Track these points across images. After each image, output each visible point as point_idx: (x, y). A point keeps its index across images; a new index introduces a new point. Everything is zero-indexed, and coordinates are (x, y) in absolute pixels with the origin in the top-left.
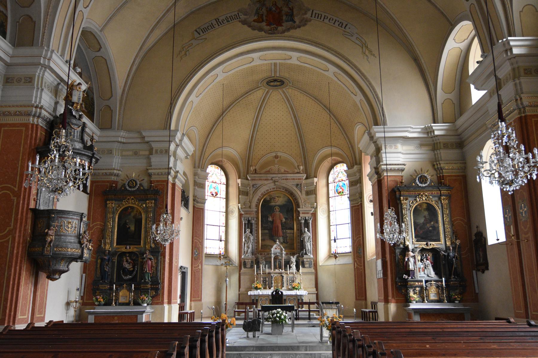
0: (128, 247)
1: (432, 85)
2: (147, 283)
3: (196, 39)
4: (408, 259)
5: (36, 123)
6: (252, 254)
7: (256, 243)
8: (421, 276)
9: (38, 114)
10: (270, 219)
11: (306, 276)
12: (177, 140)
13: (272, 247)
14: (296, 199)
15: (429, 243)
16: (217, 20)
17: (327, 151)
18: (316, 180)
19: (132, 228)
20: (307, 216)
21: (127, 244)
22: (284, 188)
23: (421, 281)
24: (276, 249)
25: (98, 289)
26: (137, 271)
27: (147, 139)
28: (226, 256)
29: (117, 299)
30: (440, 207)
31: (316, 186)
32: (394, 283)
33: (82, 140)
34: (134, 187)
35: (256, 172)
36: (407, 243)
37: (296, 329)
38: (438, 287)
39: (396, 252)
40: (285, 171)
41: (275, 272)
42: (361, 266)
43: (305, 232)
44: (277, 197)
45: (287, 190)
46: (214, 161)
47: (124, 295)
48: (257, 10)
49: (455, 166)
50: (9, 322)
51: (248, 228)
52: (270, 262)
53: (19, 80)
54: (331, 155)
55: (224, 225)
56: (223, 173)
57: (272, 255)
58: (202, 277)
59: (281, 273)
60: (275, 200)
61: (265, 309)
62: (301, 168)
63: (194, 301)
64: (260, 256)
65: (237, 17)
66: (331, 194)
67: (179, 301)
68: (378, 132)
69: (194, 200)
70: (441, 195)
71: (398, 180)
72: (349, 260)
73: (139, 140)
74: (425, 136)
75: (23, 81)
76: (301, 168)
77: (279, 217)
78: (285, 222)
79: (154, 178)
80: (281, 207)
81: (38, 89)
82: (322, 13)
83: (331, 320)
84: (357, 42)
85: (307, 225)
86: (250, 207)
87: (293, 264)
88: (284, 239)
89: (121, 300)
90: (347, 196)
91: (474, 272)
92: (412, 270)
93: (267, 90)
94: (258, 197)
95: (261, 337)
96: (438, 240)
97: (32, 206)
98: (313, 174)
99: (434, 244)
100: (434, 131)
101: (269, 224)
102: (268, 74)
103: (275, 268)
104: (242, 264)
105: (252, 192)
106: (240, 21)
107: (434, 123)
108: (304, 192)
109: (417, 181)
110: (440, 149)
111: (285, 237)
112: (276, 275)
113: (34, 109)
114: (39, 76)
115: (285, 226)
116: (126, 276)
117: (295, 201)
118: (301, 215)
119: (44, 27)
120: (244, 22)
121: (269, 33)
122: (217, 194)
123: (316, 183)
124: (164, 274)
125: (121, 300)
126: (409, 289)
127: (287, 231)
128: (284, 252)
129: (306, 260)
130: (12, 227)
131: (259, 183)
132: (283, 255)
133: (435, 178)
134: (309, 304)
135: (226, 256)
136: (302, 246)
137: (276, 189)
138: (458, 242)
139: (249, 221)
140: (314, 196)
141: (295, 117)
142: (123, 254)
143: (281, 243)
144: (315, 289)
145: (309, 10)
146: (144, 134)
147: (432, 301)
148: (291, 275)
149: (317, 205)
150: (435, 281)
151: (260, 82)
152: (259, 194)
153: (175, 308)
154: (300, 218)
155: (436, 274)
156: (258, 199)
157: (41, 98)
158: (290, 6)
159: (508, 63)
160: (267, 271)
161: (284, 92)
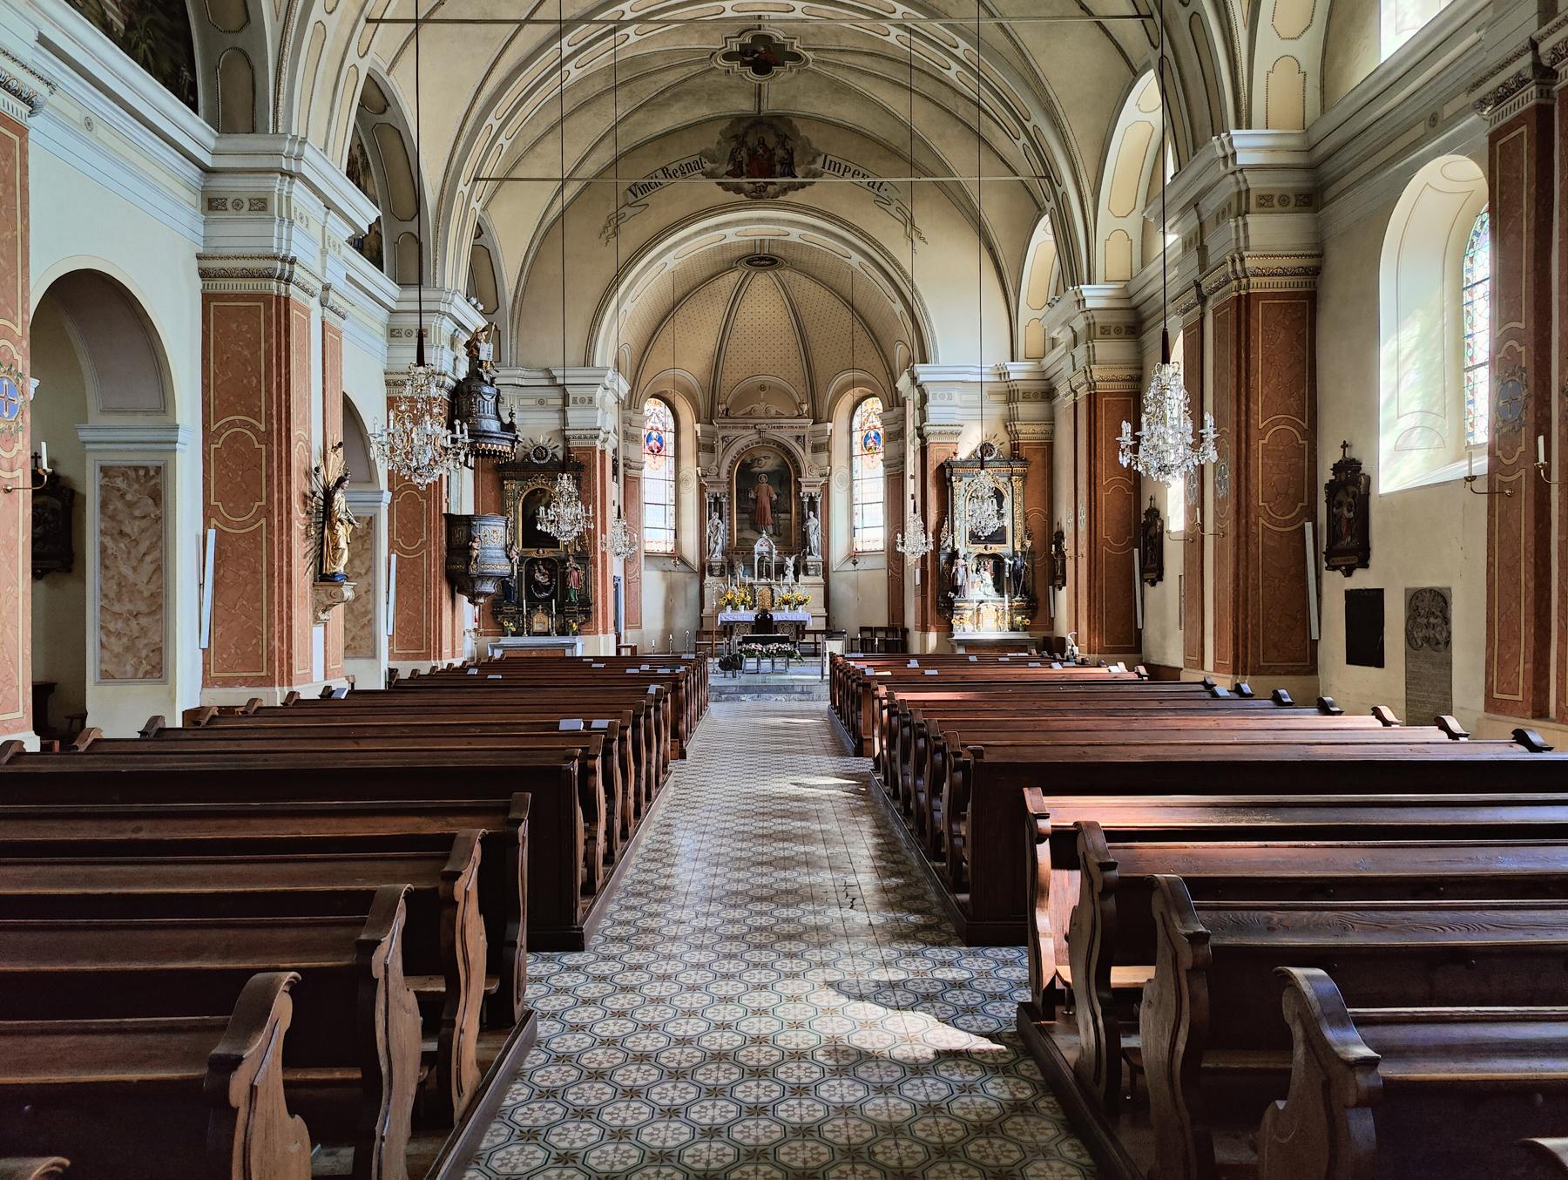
0: (541, 551)
1: (1012, 294)
3: (630, 206)
5: (276, 292)
7: (729, 535)
9: (286, 274)
10: (752, 495)
13: (755, 542)
14: (795, 462)
15: (989, 546)
16: (665, 170)
17: (847, 377)
18: (830, 426)
20: (815, 491)
21: (539, 547)
26: (556, 586)
28: (677, 556)
29: (530, 625)
30: (1010, 492)
33: (499, 418)
34: (543, 459)
35: (727, 415)
36: (957, 546)
42: (898, 573)
43: (809, 517)
45: (780, 445)
46: (657, 391)
47: (540, 621)
48: (732, 153)
49: (1038, 429)
51: (715, 511)
53: (238, 205)
54: (853, 384)
56: (668, 412)
59: (770, 585)
62: (805, 407)
66: (857, 450)
67: (613, 628)
70: (1012, 475)
72: (882, 562)
73: (546, 382)
74: (997, 379)
75: (247, 205)
76: (805, 407)
77: (767, 493)
78: (777, 500)
81: (282, 220)
82: (840, 161)
84: (898, 216)
86: (718, 475)
88: (774, 529)
89: (537, 628)
90: (881, 456)
94: (731, 458)
95: (744, 677)
97: (445, 511)
98: (825, 416)
101: (750, 503)
103: (760, 576)
105: (720, 450)
108: (809, 450)
110: (1247, 212)
112: (761, 588)
114: (280, 196)
116: (541, 593)
120: (710, 175)
121: (752, 197)
124: (596, 591)
125: (537, 628)
128: (775, 552)
130: (425, 539)
131: (735, 433)
132: (774, 556)
133: (1007, 445)
134: (815, 632)
140: (827, 454)
142: (534, 561)
145: (820, 155)
150: (992, 601)
152: (733, 451)
154: (801, 494)
156: (732, 462)
157: (289, 240)
158: (789, 148)
161: (776, 275)
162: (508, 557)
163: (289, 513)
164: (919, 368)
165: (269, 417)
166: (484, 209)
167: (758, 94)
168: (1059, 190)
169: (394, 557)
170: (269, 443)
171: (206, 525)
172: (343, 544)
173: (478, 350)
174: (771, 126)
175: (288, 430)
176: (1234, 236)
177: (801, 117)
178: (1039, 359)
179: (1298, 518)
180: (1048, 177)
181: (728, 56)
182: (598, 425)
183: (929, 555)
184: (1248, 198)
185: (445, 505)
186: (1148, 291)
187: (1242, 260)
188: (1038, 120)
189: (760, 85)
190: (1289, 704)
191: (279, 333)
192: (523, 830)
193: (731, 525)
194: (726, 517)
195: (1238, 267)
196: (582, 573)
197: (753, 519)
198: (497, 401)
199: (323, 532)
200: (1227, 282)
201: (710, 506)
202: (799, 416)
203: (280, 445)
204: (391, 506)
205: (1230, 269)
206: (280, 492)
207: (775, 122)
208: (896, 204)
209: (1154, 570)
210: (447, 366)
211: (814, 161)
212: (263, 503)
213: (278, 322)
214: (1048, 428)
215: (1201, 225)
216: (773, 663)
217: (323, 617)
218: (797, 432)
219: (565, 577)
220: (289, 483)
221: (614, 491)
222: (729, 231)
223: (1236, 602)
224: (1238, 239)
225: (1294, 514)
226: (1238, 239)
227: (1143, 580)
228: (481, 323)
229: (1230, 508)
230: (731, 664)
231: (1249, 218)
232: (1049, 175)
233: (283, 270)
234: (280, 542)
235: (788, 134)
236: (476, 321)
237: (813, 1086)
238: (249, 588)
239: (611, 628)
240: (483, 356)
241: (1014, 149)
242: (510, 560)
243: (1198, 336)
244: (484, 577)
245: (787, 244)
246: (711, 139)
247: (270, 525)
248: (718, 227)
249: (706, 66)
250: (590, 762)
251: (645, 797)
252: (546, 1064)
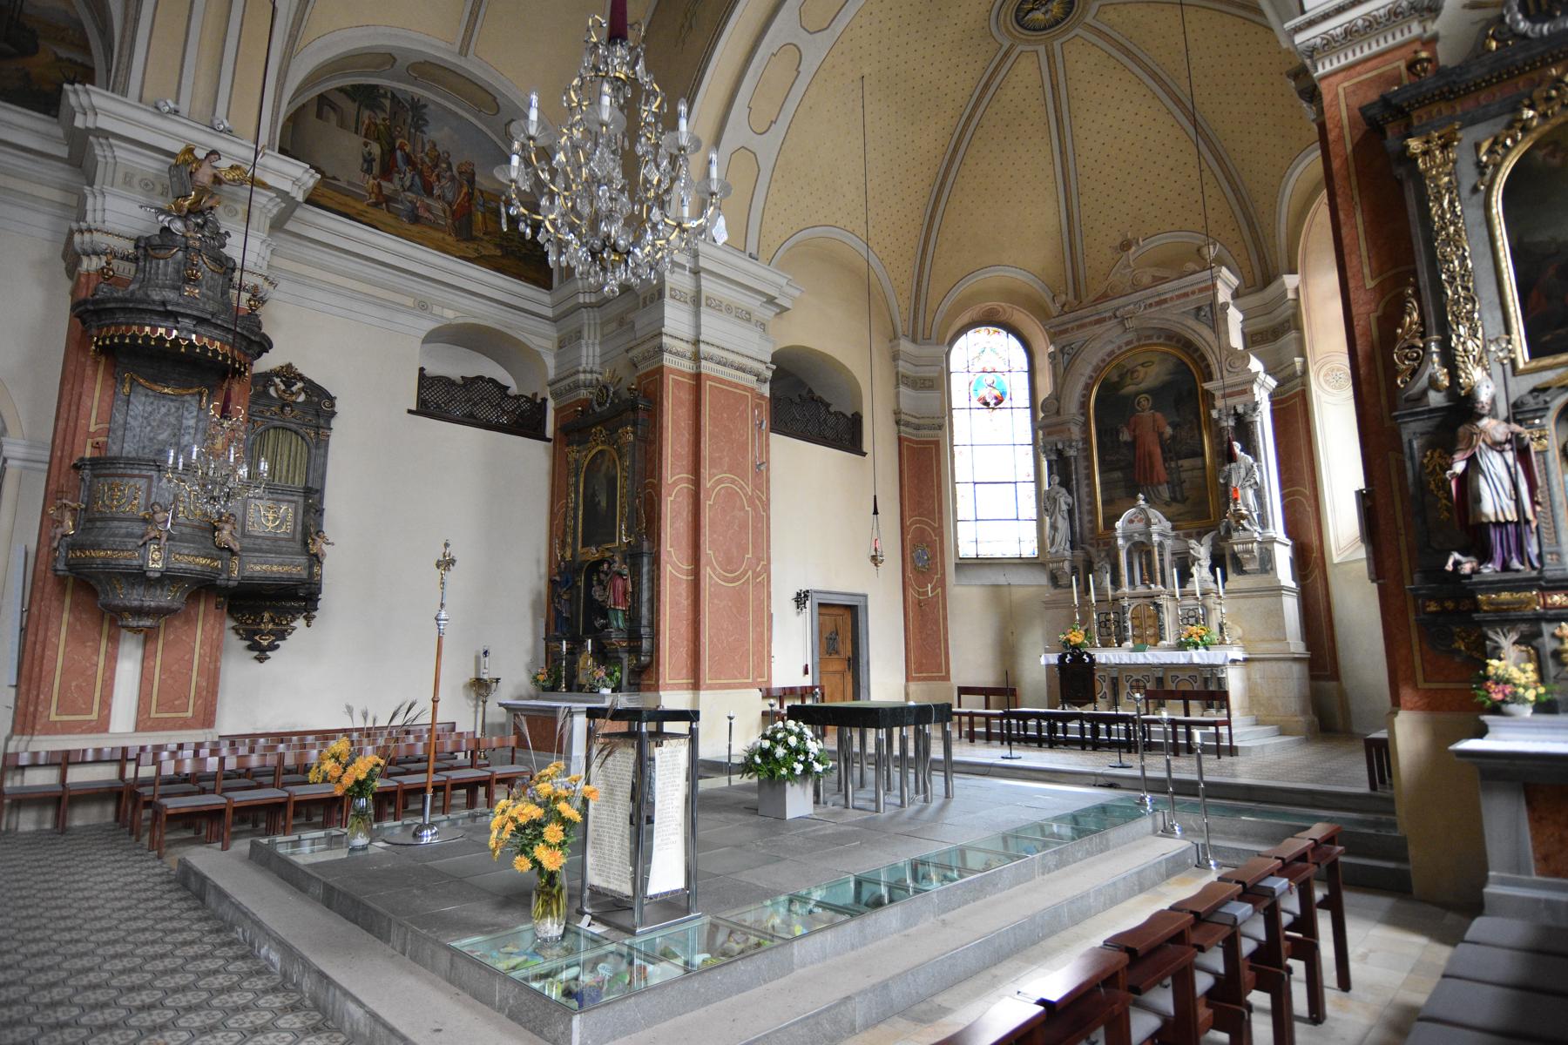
4: (1473, 462)
6: (1072, 547)
10: (1125, 436)
11: (1250, 600)
18: (1290, 281)
19: (604, 504)
22: (1161, 332)
24: (1131, 521)
31: (1297, 300)
39: (1405, 438)
44: (1142, 365)
55: (1032, 479)
57: (1120, 542)
58: (945, 618)
60: (1135, 375)
63: (915, 679)
77: (1154, 424)
78: (1173, 437)
80: (1155, 393)
87: (1200, 566)
88: (1173, 491)
92: (1498, 524)
93: (1006, 45)
111: (1175, 484)
115: (1172, 451)
117: (1203, 365)
118: (1219, 403)
122: (999, 400)
123: (1297, 290)
126: (1491, 634)
127: (1180, 462)
129: (1240, 547)
137: (1136, 344)
139: (1060, 453)
149: (1305, 364)
151: (994, 29)
216: (1169, 771)
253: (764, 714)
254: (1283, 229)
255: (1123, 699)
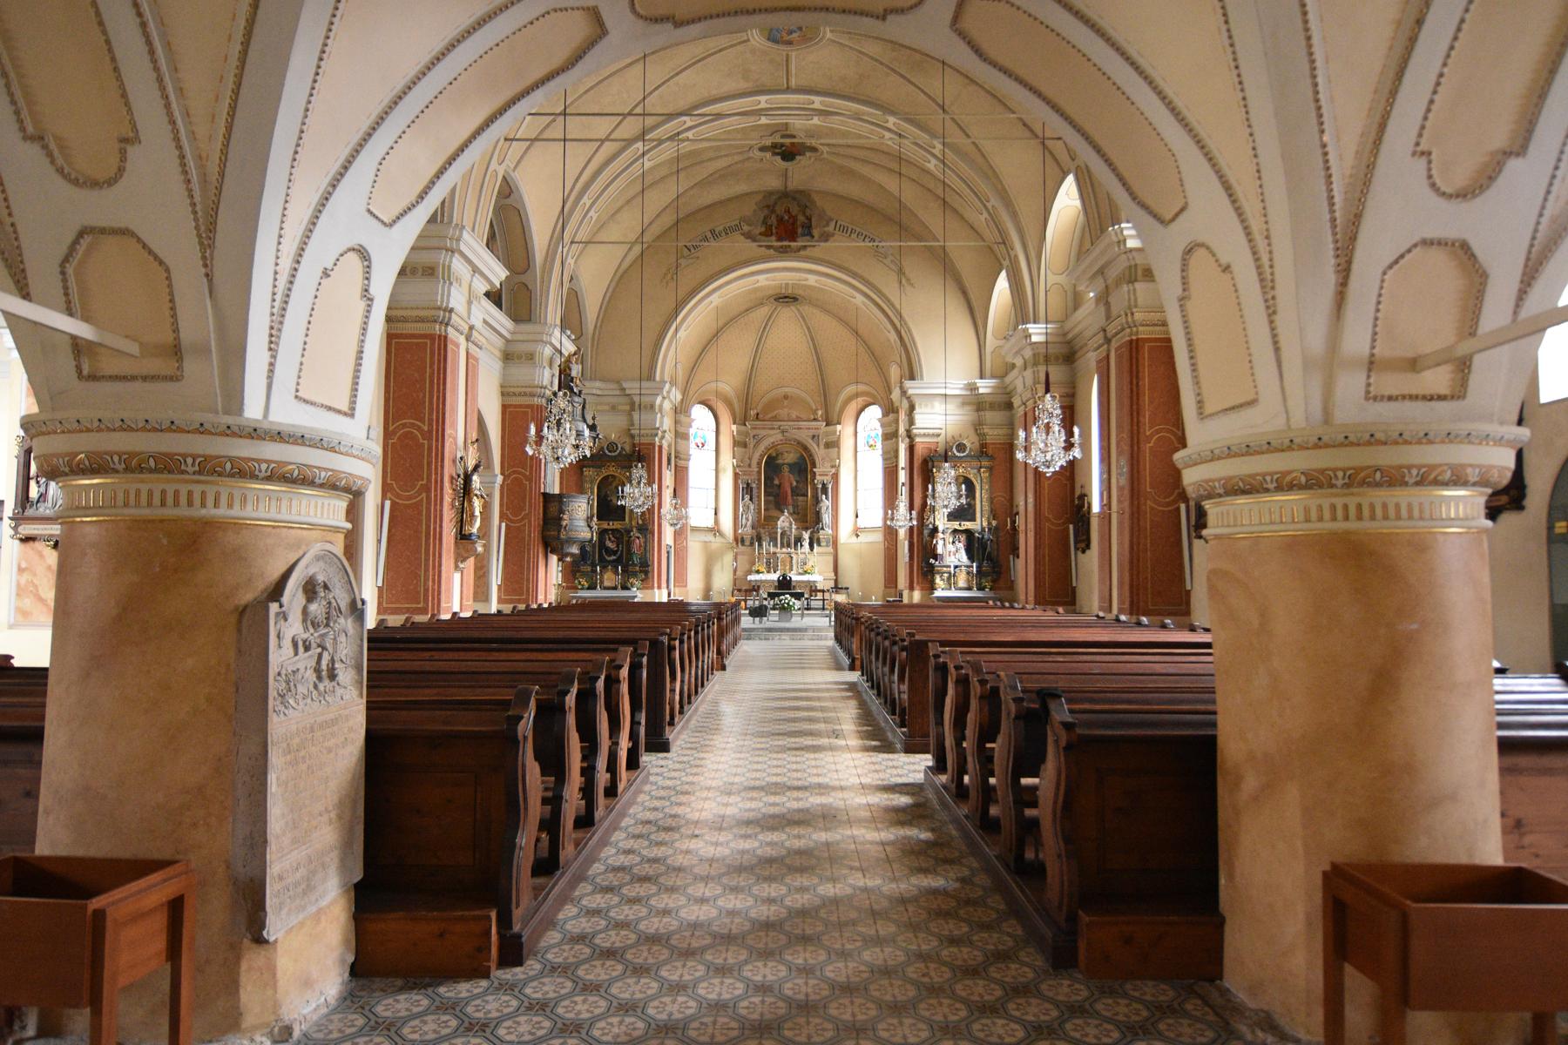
2: (636, 565)
8: (951, 561)
10: (776, 482)
12: (665, 393)
15: (963, 523)
17: (852, 389)
18: (839, 427)
22: (795, 440)
23: (950, 567)
25: (579, 571)
26: (622, 551)
27: (628, 392)
28: (715, 530)
29: (602, 582)
32: (920, 568)
33: (585, 421)
36: (937, 523)
37: (805, 619)
38: (968, 573)
40: (797, 417)
41: (781, 552)
46: (703, 398)
47: (609, 578)
48: (765, 218)
50: (433, 609)
52: (776, 539)
53: (520, 357)
54: (857, 395)
61: (772, 596)
62: (820, 413)
64: (762, 531)
65: (737, 228)
68: (913, 388)
69: (676, 457)
71: (933, 447)
72: (878, 537)
73: (618, 393)
74: (969, 393)
76: (820, 413)
77: (789, 480)
79: (637, 440)
80: (791, 466)
83: (623, 507)
85: (825, 490)
86: (750, 466)
89: (607, 584)
90: (880, 452)
91: (1011, 557)
96: (973, 519)
97: (542, 491)
98: (835, 420)
99: (968, 525)
100: (1030, 336)
102: (778, 291)
103: (782, 546)
104: (739, 540)
105: (752, 446)
106: (742, 234)
107: (981, 378)
108: (822, 447)
109: (954, 450)
110: (1136, 280)
111: (796, 506)
113: (442, 313)
116: (610, 556)
118: (818, 477)
119: (541, 296)
120: (748, 236)
124: (653, 555)
128: (794, 526)
131: (763, 433)
133: (977, 444)
135: (715, 530)
136: (818, 518)
138: (994, 523)
139: (748, 484)
141: (812, 339)
143: (790, 514)
144: (833, 574)
145: (832, 220)
146: (625, 385)
147: (961, 589)
148: (803, 556)
152: (762, 448)
153: (665, 592)
155: (969, 558)
157: (449, 295)
159: (1029, 348)
160: (772, 549)
161: (798, 310)
162: (589, 526)
163: (442, 489)
164: (908, 384)
165: (430, 420)
166: (575, 262)
167: (785, 175)
168: (1012, 253)
169: (504, 525)
170: (430, 439)
171: (384, 497)
172: (477, 513)
173: (570, 369)
174: (794, 199)
175: (443, 430)
176: (1126, 297)
177: (816, 192)
178: (1002, 377)
179: (1175, 501)
180: (1004, 243)
181: (762, 149)
182: (657, 425)
183: (915, 529)
184: (1136, 272)
185: (542, 486)
186: (1076, 331)
187: (1132, 314)
188: (994, 202)
189: (787, 55)
190: (1146, 626)
191: (439, 361)
192: (645, 660)
193: (760, 505)
194: (755, 499)
195: (1130, 319)
196: (642, 540)
197: (777, 500)
198: (584, 407)
199: (463, 504)
200: (1123, 329)
201: (744, 489)
202: (815, 420)
203: (437, 440)
204: (502, 487)
205: (1124, 321)
206: (436, 474)
207: (797, 196)
208: (891, 258)
209: (1084, 543)
210: (546, 382)
211: (827, 225)
212: (424, 482)
213: (439, 354)
214: (1009, 431)
215: (1107, 287)
217: (461, 566)
218: (811, 432)
219: (629, 544)
220: (442, 467)
221: (668, 478)
222: (761, 277)
223: (1131, 562)
224: (1129, 299)
225: (1171, 498)
226: (1129, 299)
227: (1076, 549)
228: (572, 349)
229: (1127, 492)
230: (759, 612)
231: (1137, 285)
232: (1005, 242)
233: (444, 317)
234: (435, 510)
235: (808, 204)
236: (569, 347)
237: (818, 967)
238: (412, 543)
239: (664, 585)
240: (574, 374)
241: (981, 219)
242: (591, 528)
243: (1106, 367)
244: (571, 541)
245: (809, 287)
246: (749, 208)
247: (428, 498)
248: (753, 274)
249: (746, 156)
250: (672, 643)
251: (700, 683)
252: (607, 928)
253: (923, 645)
254: (837, 409)
255: (261, 506)
